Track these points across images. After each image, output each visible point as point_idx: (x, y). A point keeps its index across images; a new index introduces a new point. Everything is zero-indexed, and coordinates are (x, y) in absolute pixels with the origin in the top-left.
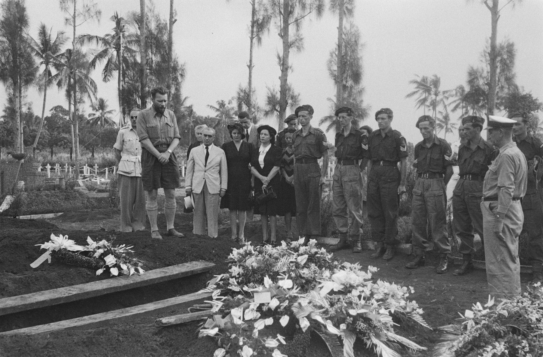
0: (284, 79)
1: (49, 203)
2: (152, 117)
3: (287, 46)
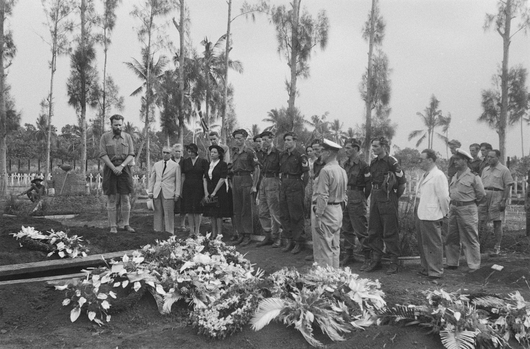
0: (291, 101)
1: (73, 206)
2: (111, 138)
3: (295, 74)
